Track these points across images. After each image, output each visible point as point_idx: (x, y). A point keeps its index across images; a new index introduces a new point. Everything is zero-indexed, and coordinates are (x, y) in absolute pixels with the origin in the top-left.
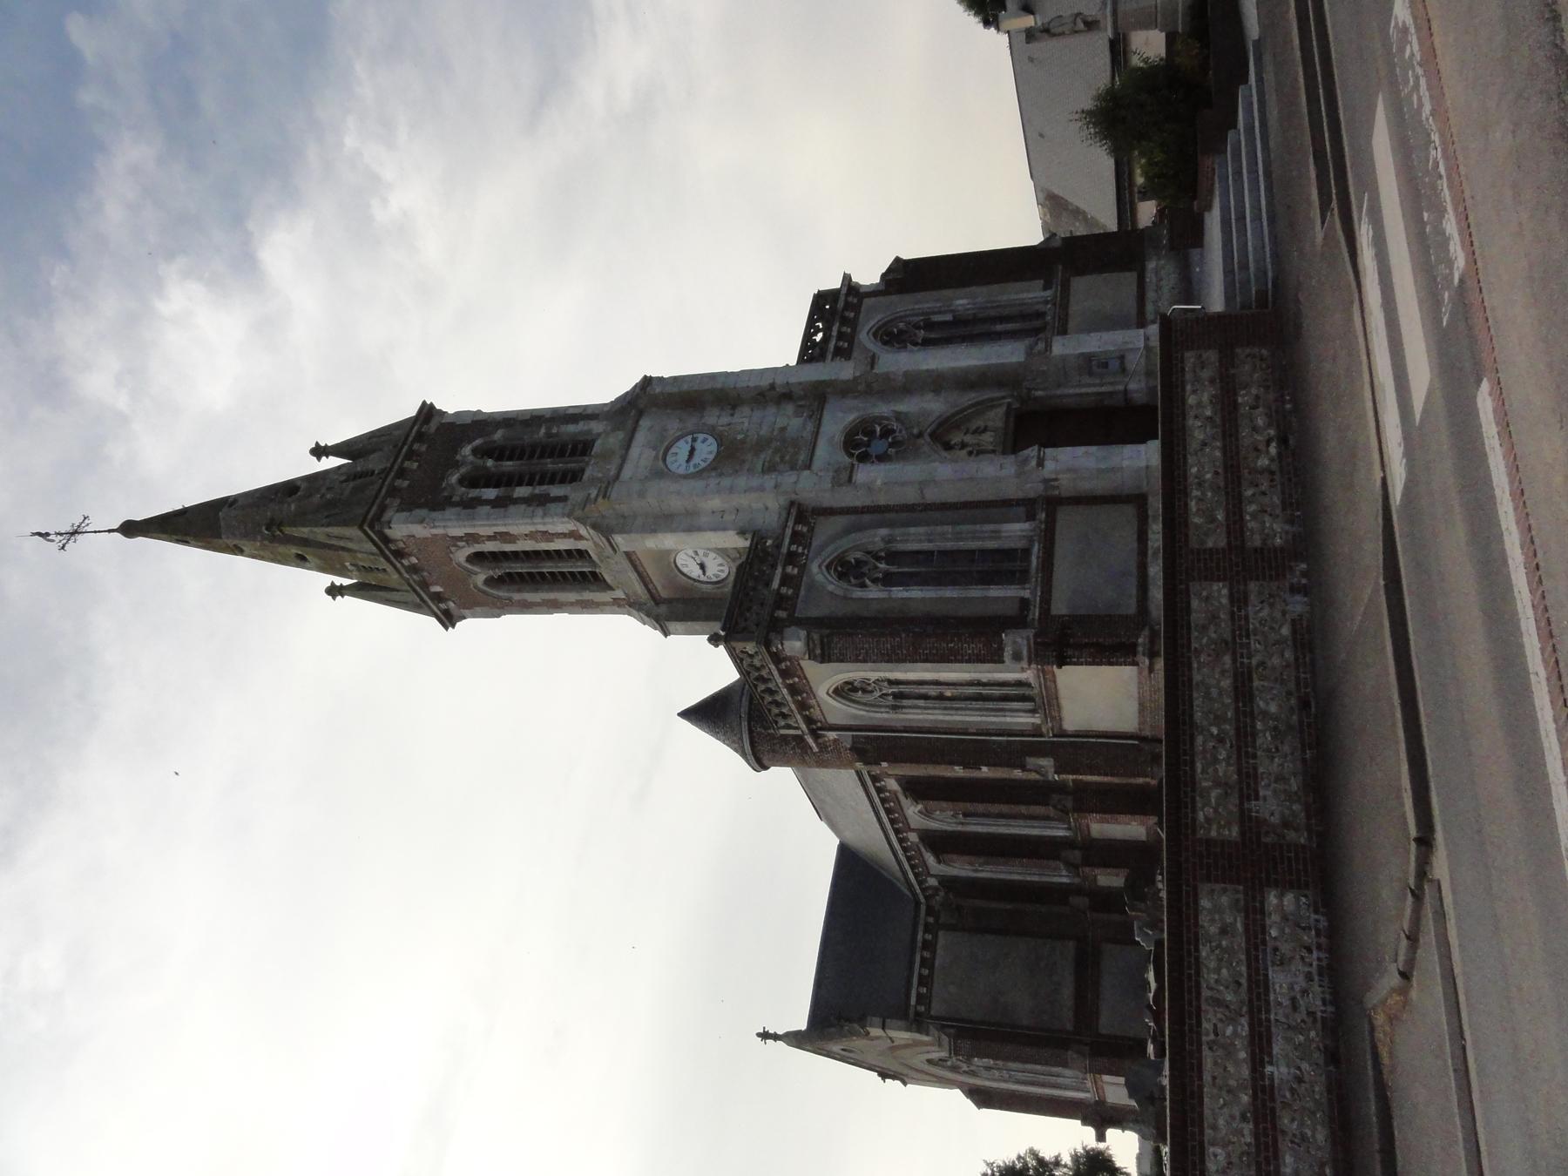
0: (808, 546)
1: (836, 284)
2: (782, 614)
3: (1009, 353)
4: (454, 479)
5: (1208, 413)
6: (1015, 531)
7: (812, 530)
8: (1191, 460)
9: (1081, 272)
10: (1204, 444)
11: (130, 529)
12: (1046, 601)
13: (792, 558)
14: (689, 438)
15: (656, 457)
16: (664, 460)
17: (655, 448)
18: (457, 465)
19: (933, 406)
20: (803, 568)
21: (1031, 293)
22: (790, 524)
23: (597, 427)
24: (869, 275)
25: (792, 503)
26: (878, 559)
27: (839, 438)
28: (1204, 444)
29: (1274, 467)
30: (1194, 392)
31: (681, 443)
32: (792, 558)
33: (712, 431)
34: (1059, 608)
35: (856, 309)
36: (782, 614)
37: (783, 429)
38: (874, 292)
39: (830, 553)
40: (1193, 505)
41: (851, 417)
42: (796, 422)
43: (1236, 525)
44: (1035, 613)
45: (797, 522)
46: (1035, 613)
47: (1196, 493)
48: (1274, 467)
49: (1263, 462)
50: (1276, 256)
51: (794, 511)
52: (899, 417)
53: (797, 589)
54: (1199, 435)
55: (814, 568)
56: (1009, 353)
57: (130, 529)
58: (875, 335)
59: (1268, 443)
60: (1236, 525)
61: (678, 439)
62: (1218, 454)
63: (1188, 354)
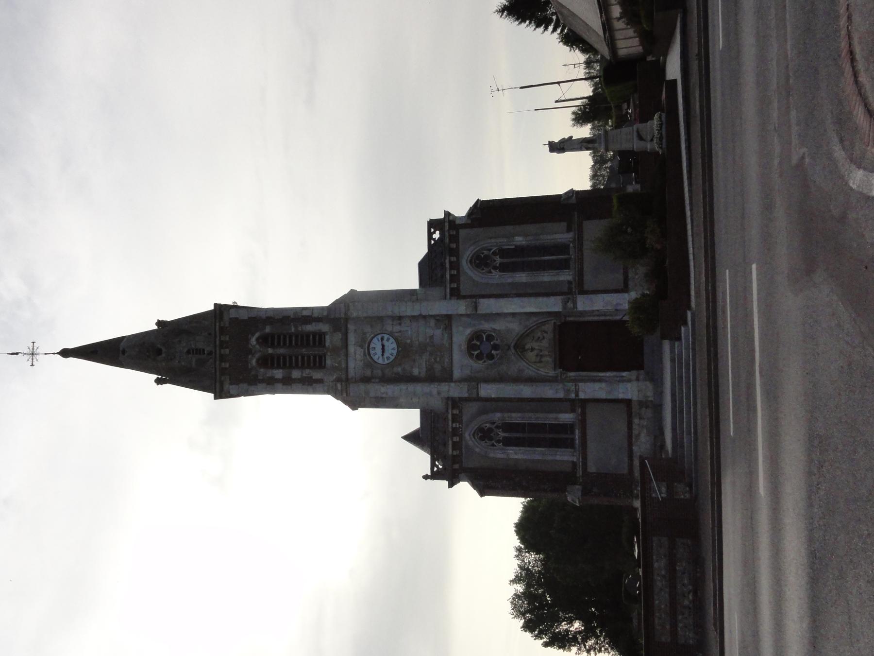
0: (461, 422)
1: (441, 216)
2: (456, 466)
3: (553, 304)
4: (254, 362)
5: (663, 573)
6: (566, 417)
7: (461, 411)
8: (655, 597)
9: (589, 218)
10: (661, 589)
11: (66, 353)
12: (585, 464)
13: (455, 432)
14: (379, 337)
15: (365, 355)
16: (369, 354)
17: (361, 347)
18: (250, 352)
19: (516, 327)
20: (461, 437)
21: (558, 234)
22: (450, 411)
23: (324, 327)
24: (460, 210)
25: (448, 398)
26: (498, 427)
27: (464, 347)
28: (661, 589)
29: (691, 606)
30: (657, 561)
31: (375, 340)
32: (455, 432)
33: (391, 334)
34: (592, 468)
35: (454, 239)
36: (456, 466)
37: (432, 337)
38: (464, 226)
39: (474, 426)
40: (657, 621)
41: (468, 331)
42: (438, 332)
43: (674, 632)
44: (580, 473)
45: (453, 408)
46: (580, 473)
47: (657, 614)
48: (691, 606)
49: (686, 603)
50: (696, 451)
51: (450, 403)
52: (494, 330)
53: (460, 449)
54: (659, 584)
55: (467, 436)
56: (553, 304)
57: (66, 353)
58: (471, 262)
59: (689, 593)
60: (674, 632)
61: (373, 338)
62: (667, 595)
63: (655, 539)
